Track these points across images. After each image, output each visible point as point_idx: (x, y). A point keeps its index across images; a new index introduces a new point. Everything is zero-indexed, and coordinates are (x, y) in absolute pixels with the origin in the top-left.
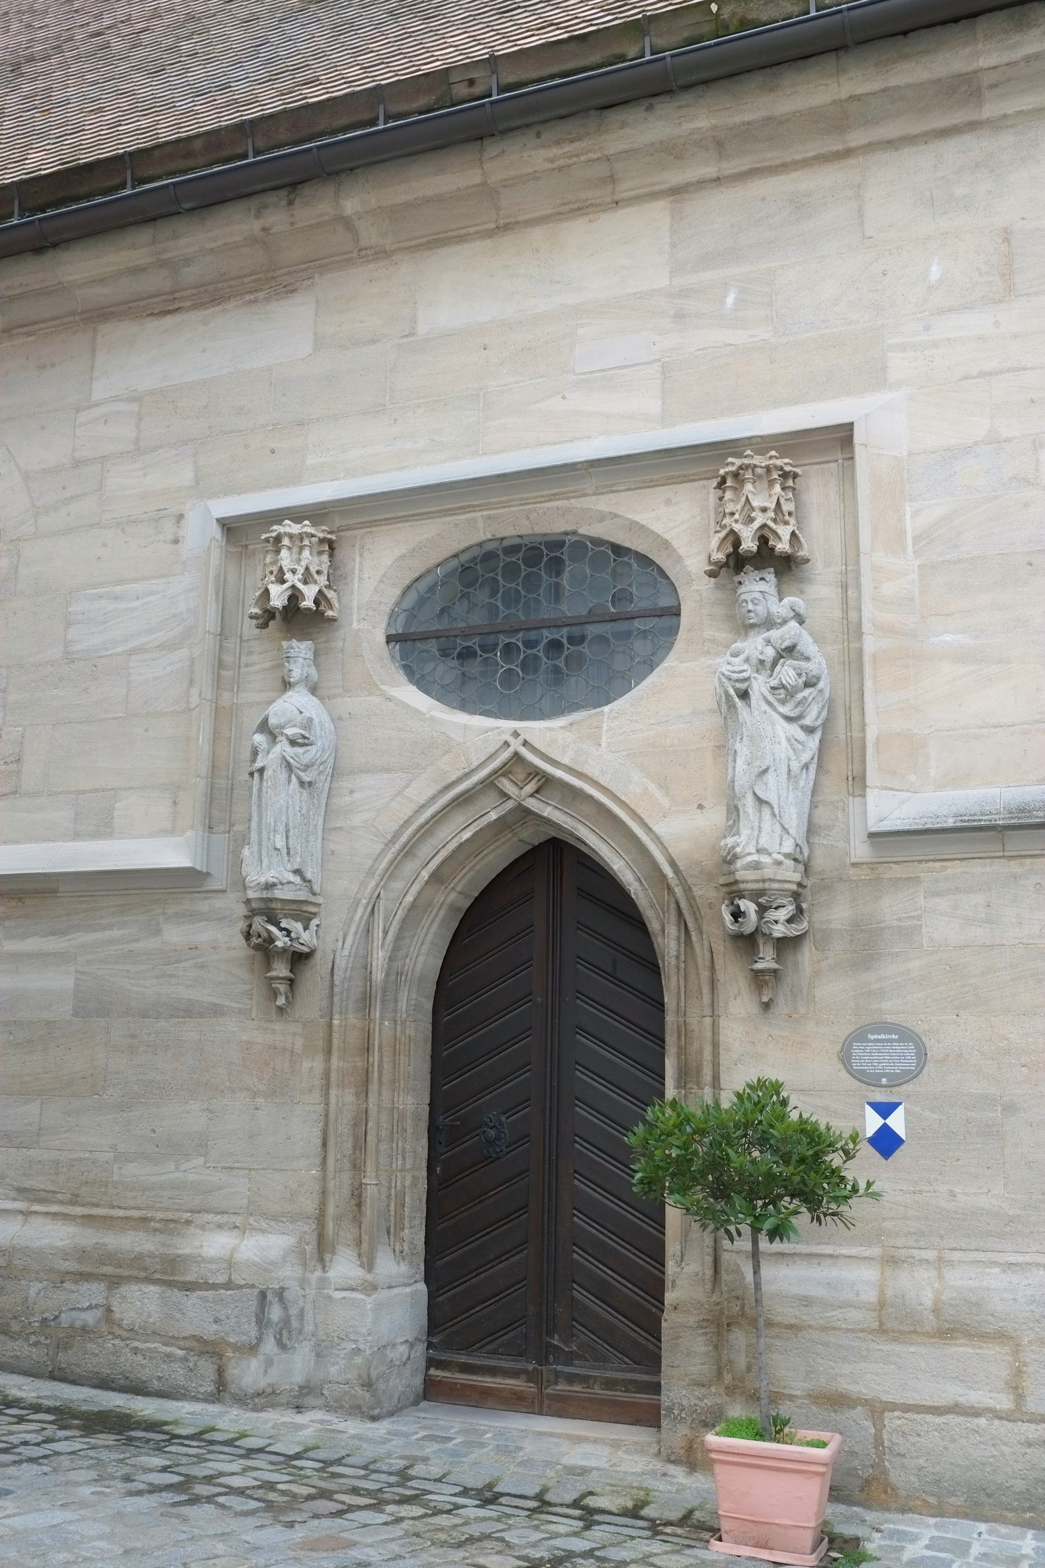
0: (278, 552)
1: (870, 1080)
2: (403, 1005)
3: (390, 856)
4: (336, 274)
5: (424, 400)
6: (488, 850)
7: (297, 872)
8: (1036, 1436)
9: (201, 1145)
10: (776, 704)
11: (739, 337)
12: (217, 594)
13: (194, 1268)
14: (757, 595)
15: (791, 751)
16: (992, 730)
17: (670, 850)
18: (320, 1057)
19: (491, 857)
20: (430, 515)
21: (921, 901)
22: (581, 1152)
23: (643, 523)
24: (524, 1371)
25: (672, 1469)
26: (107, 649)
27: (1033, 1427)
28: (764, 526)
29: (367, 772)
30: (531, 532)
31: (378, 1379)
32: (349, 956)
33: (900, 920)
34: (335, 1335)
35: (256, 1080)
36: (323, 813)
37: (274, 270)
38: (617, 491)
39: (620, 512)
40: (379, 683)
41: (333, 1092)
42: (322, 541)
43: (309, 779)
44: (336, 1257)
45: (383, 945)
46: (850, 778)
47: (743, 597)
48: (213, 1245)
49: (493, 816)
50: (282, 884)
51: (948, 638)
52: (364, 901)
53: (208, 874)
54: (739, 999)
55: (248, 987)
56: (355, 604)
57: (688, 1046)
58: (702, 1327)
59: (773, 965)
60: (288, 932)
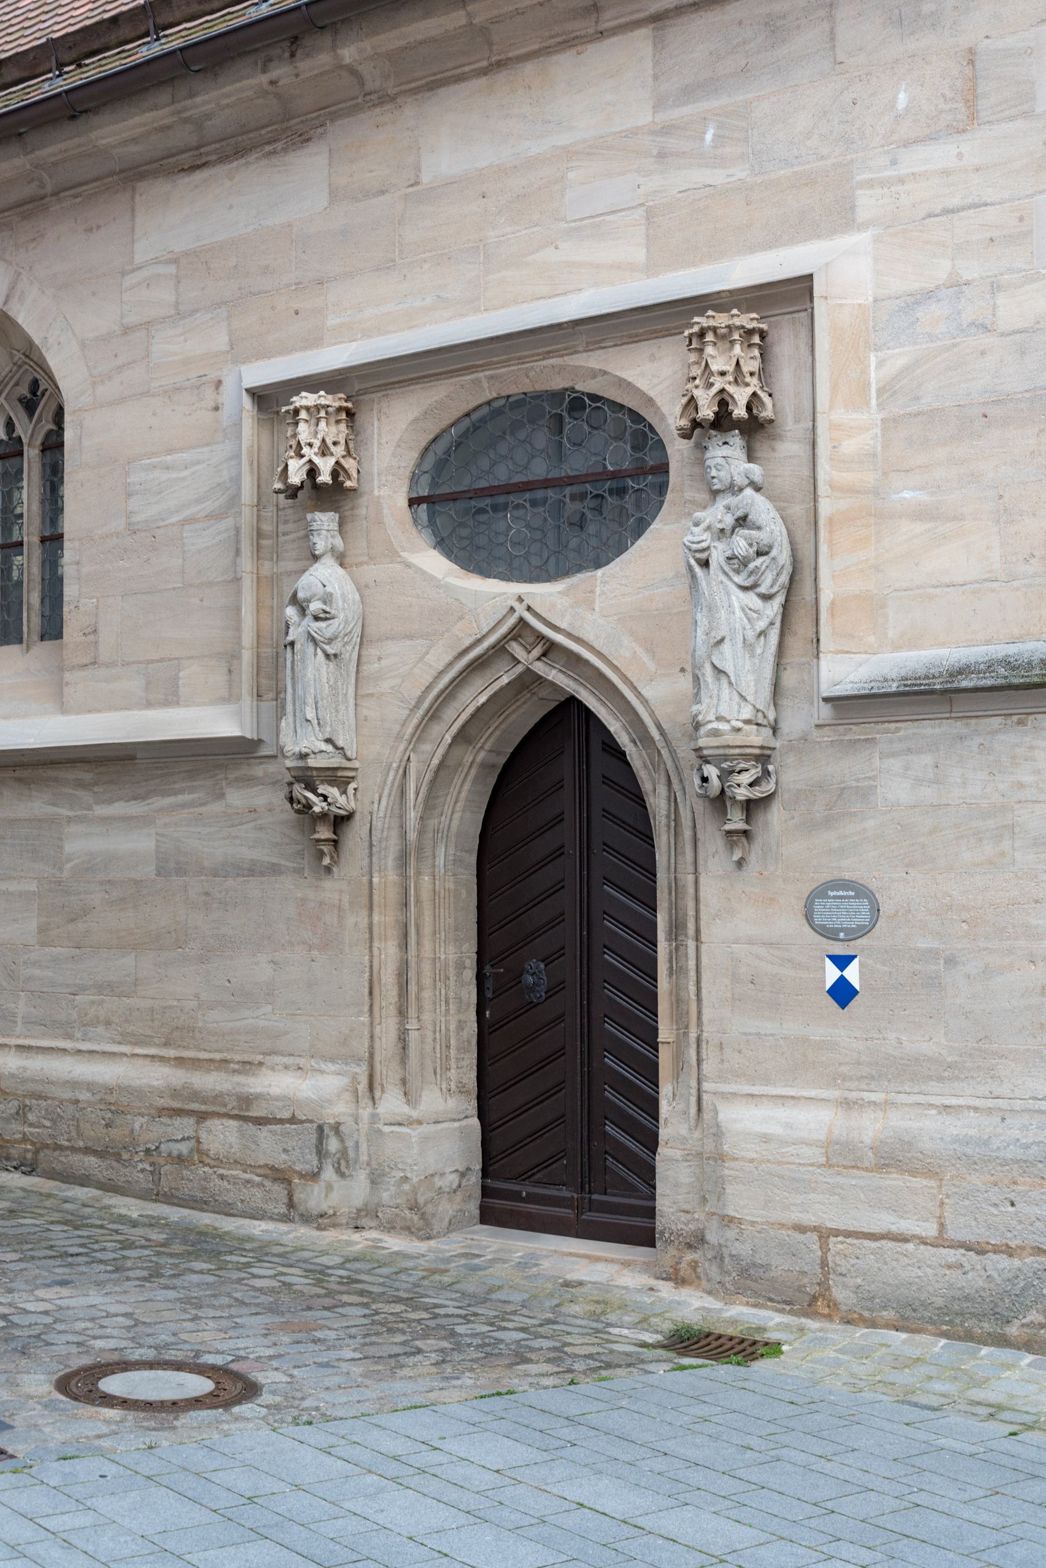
0: (297, 424)
1: (829, 933)
2: (440, 861)
4: (346, 120)
5: (429, 254)
6: (510, 710)
7: (329, 741)
8: (954, 1259)
9: (268, 994)
10: (731, 574)
11: (717, 177)
12: (252, 464)
13: (264, 1104)
14: (720, 461)
15: (746, 621)
16: (947, 589)
18: (365, 913)
19: (514, 716)
21: (877, 762)
23: (630, 380)
25: (660, 1284)
26: (163, 520)
27: (952, 1251)
28: (722, 391)
29: (393, 638)
31: (426, 1204)
32: (385, 817)
33: (858, 780)
34: (386, 1164)
35: (310, 934)
36: (353, 681)
37: (288, 120)
38: (605, 347)
40: (399, 550)
41: (376, 944)
42: (340, 409)
43: (333, 652)
44: (386, 1095)
45: (415, 806)
48: (277, 1084)
49: (505, 680)
50: (315, 753)
51: (907, 495)
52: (395, 765)
53: (260, 741)
54: (717, 857)
55: (300, 847)
57: (679, 901)
58: (687, 1161)
59: (741, 826)
60: (325, 798)
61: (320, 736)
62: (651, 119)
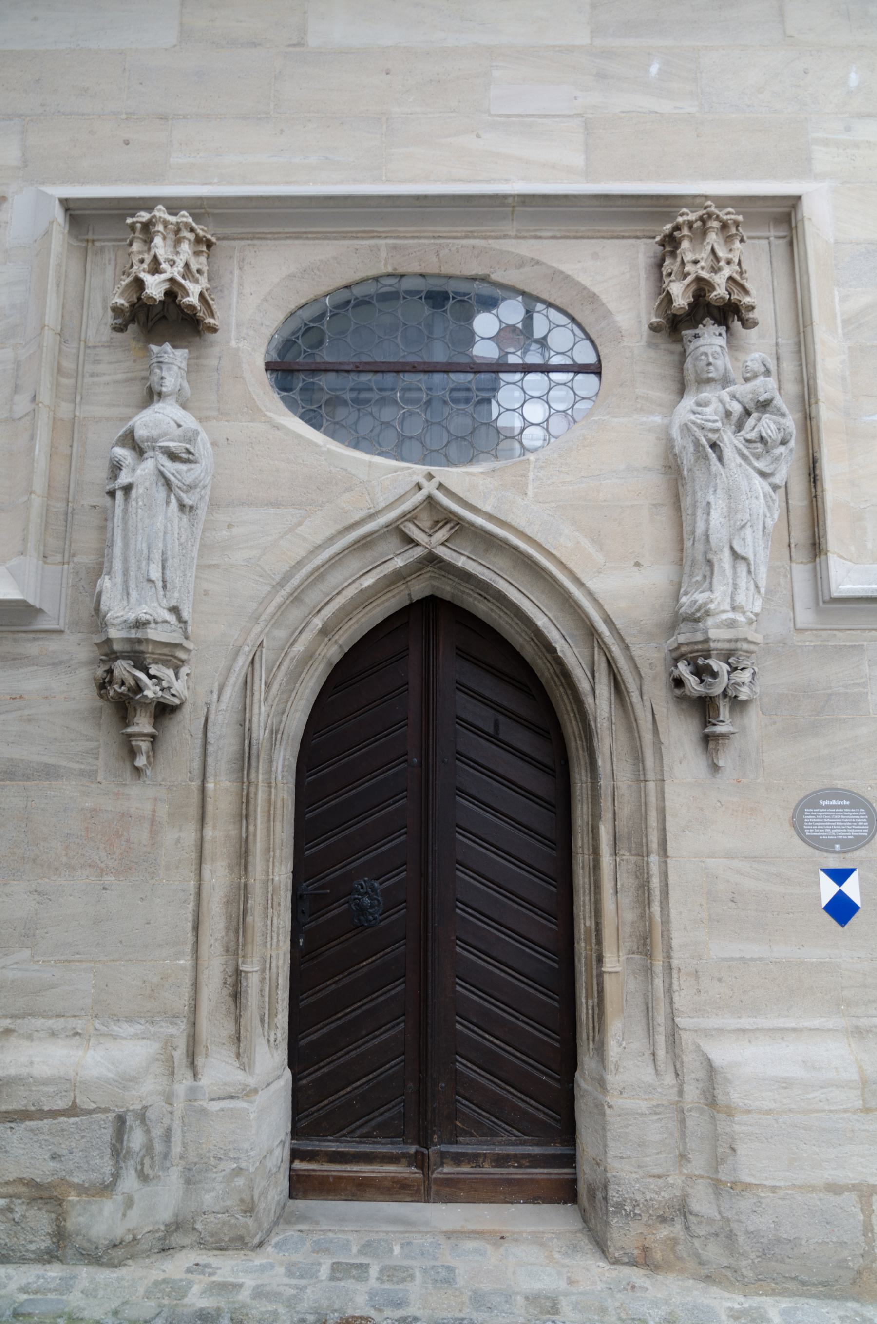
3: (278, 599)
7: (175, 610)
10: (751, 458)
17: (606, 607)
20: (326, 236)
22: (464, 918)
23: (570, 273)
24: (405, 1155)
30: (437, 271)
38: (540, 237)
39: (543, 259)
40: (263, 409)
45: (266, 699)
46: (793, 545)
47: (702, 349)
50: (156, 622)
53: (40, 611)
56: (233, 321)
58: (656, 1113)
59: (732, 729)
61: (164, 603)
62: (589, 42)
